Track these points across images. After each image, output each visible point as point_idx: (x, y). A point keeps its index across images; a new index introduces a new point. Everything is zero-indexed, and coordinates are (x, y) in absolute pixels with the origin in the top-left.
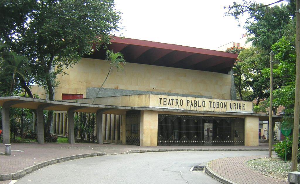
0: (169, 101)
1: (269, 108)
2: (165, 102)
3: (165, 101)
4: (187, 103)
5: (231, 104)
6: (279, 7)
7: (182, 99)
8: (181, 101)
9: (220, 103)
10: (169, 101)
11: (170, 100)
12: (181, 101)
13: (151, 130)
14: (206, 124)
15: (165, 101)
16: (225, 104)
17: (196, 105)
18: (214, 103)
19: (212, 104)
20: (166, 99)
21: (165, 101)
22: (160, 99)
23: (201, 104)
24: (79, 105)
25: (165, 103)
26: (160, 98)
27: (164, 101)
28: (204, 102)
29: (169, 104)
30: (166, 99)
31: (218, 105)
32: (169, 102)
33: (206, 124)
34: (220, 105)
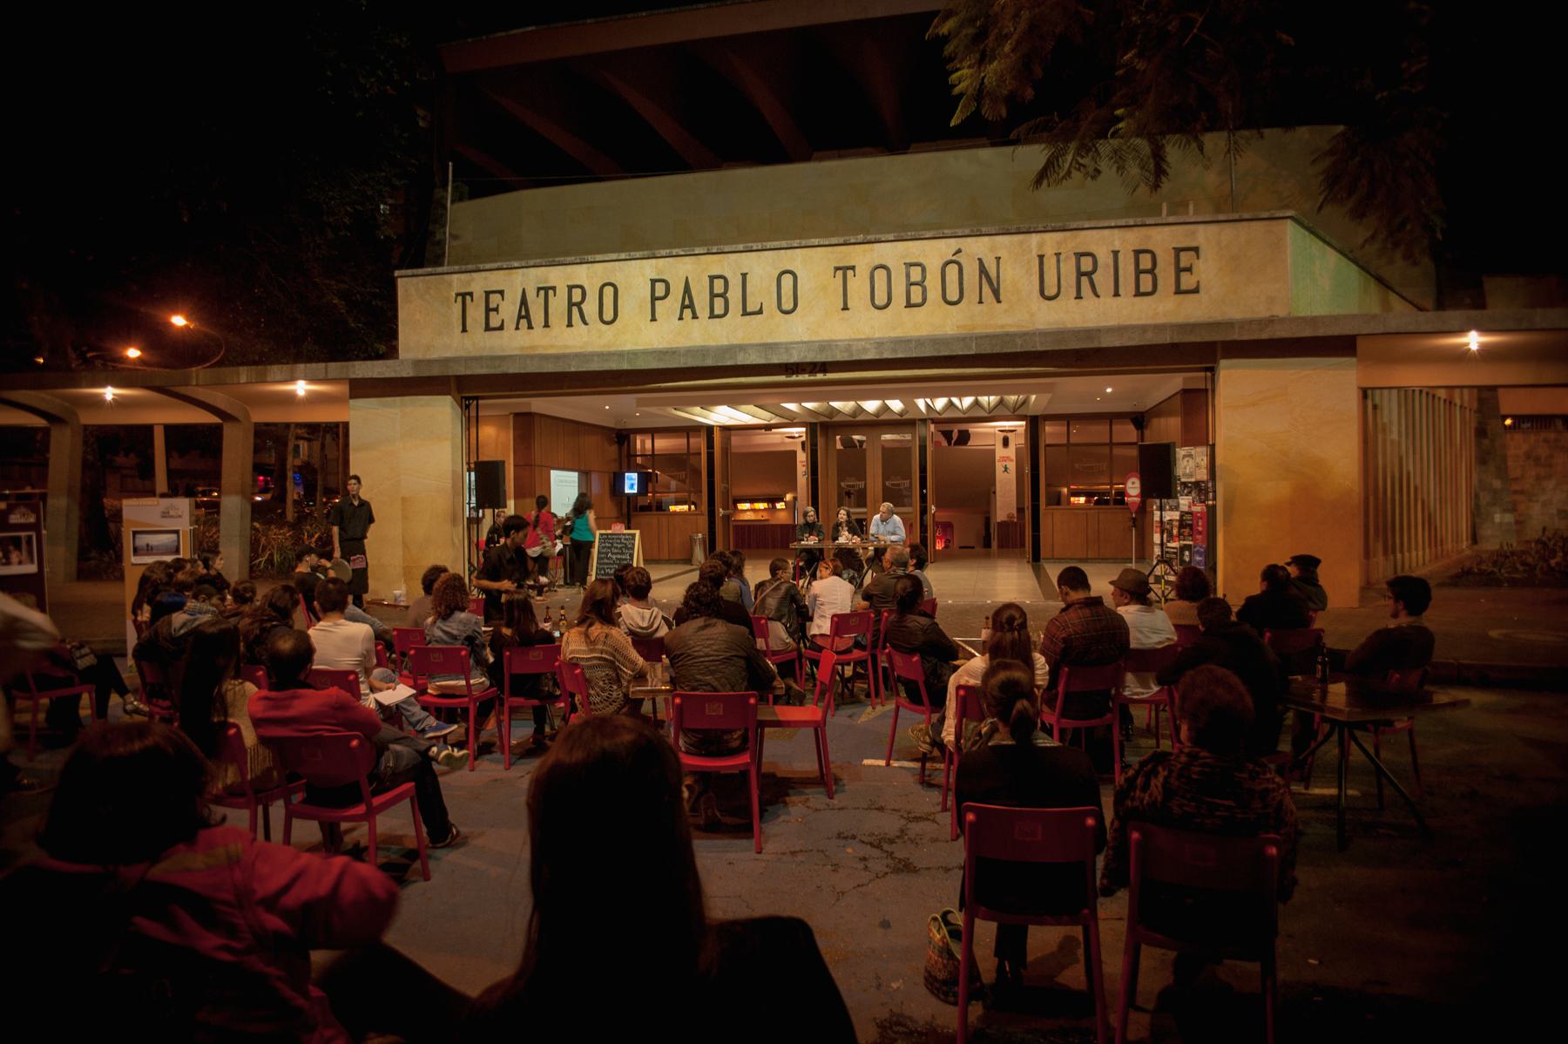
0: (524, 302)
1: (1301, 827)
2: (492, 314)
3: (496, 310)
4: (654, 299)
5: (1050, 264)
6: (693, 587)
7: (877, 263)
8: (609, 291)
9: (1104, 258)
10: (524, 302)
11: (531, 295)
12: (609, 291)
13: (404, 499)
14: (573, 476)
15: (492, 305)
16: (983, 271)
17: (719, 310)
18: (880, 275)
19: (859, 285)
20: (501, 292)
21: (492, 305)
22: (845, 270)
23: (763, 290)
24: (332, 365)
25: (494, 322)
26: (546, 289)
27: (488, 310)
28: (787, 281)
29: (688, 312)
30: (501, 292)
31: (723, 296)
32: (524, 314)
33: (573, 476)
34: (933, 283)
